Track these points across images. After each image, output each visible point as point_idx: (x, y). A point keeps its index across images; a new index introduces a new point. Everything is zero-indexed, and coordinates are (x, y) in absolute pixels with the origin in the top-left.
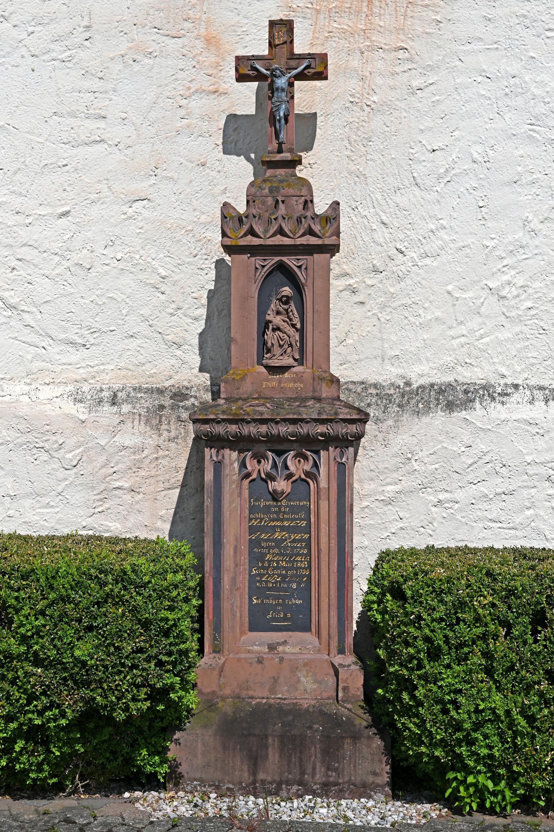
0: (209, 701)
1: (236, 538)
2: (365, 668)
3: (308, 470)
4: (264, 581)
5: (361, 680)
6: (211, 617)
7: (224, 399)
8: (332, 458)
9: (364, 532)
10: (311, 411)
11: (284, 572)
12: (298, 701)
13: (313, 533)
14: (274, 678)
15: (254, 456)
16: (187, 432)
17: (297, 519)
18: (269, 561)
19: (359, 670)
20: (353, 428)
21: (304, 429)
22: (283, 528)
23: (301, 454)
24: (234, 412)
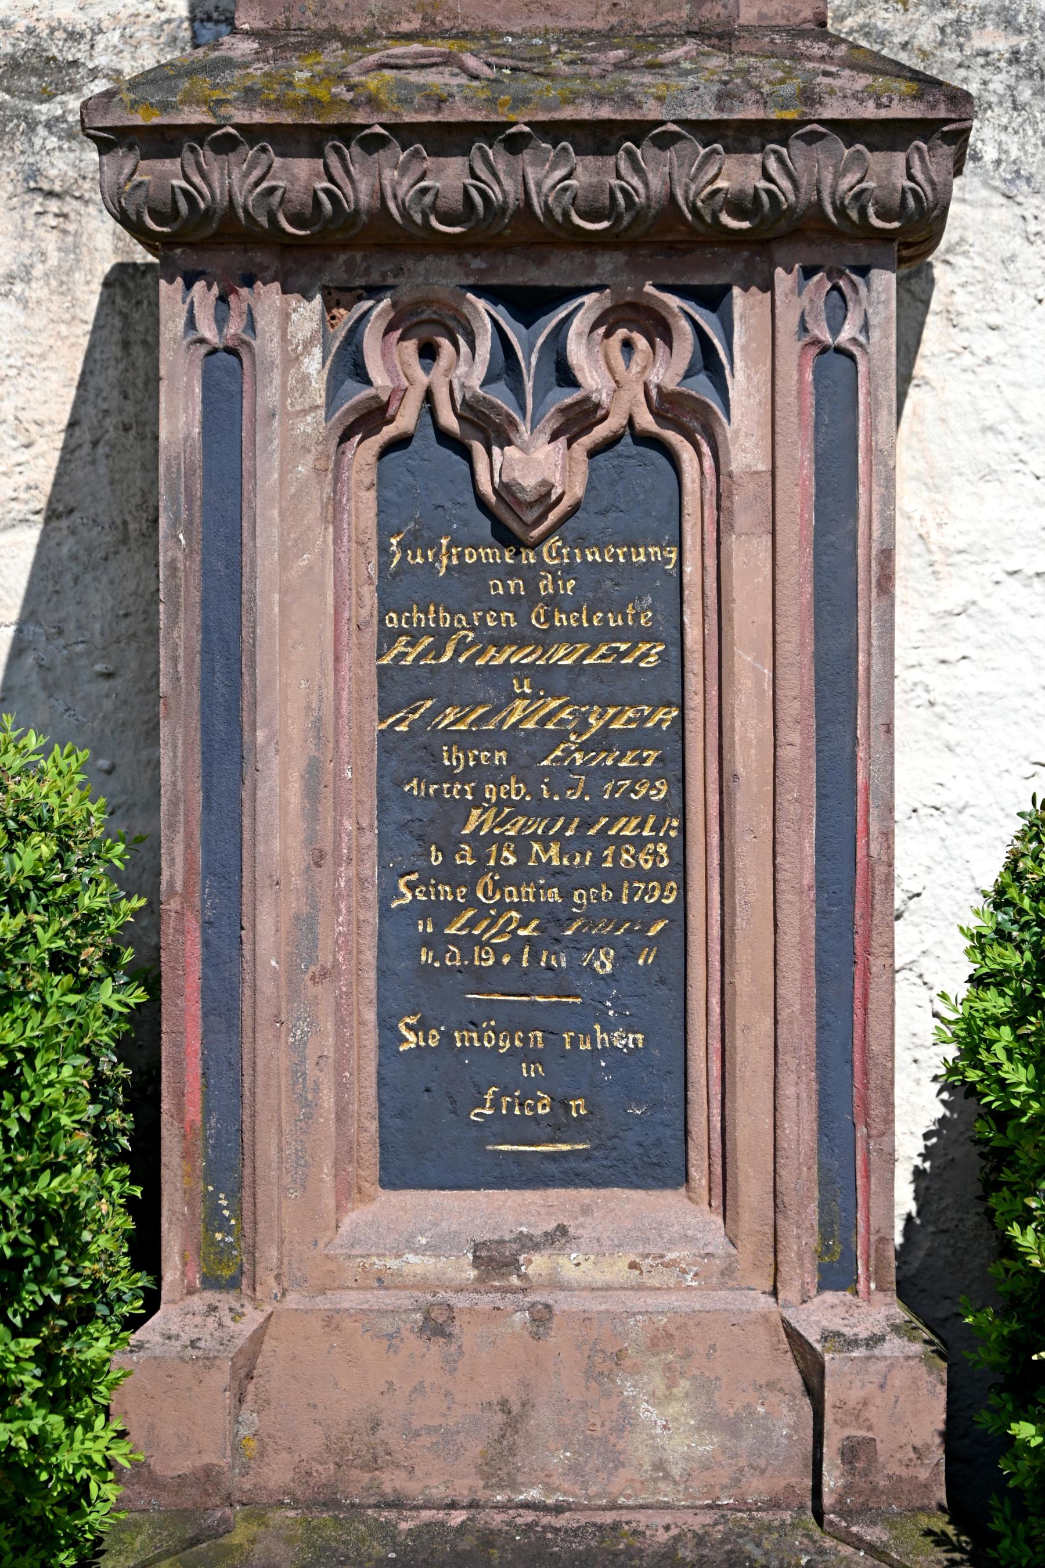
0: (183, 1515)
1: (318, 725)
2: (948, 1343)
3: (671, 386)
4: (454, 939)
5: (933, 1414)
6: (194, 1113)
7: (252, 34)
8: (788, 322)
9: (951, 735)
10: (687, 86)
11: (553, 895)
12: (625, 1516)
13: (694, 700)
14: (504, 1405)
15: (402, 323)
16: (74, 247)
17: (618, 634)
18: (480, 843)
19: (924, 1359)
20: (890, 172)
21: (650, 177)
22: (546, 680)
23: (633, 306)
24: (301, 92)
